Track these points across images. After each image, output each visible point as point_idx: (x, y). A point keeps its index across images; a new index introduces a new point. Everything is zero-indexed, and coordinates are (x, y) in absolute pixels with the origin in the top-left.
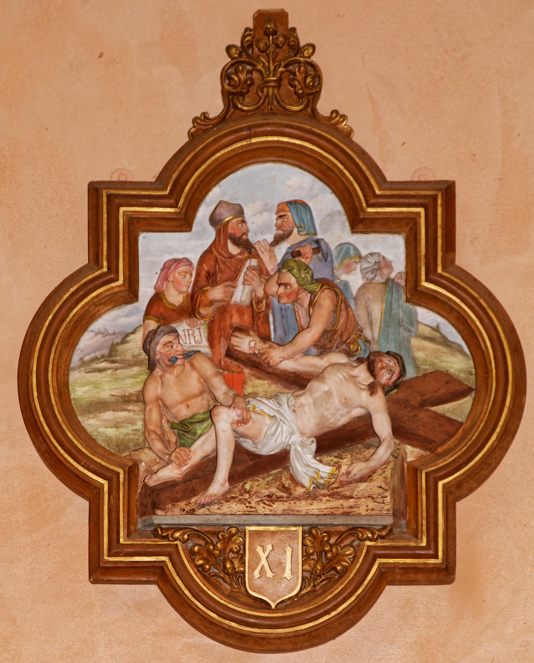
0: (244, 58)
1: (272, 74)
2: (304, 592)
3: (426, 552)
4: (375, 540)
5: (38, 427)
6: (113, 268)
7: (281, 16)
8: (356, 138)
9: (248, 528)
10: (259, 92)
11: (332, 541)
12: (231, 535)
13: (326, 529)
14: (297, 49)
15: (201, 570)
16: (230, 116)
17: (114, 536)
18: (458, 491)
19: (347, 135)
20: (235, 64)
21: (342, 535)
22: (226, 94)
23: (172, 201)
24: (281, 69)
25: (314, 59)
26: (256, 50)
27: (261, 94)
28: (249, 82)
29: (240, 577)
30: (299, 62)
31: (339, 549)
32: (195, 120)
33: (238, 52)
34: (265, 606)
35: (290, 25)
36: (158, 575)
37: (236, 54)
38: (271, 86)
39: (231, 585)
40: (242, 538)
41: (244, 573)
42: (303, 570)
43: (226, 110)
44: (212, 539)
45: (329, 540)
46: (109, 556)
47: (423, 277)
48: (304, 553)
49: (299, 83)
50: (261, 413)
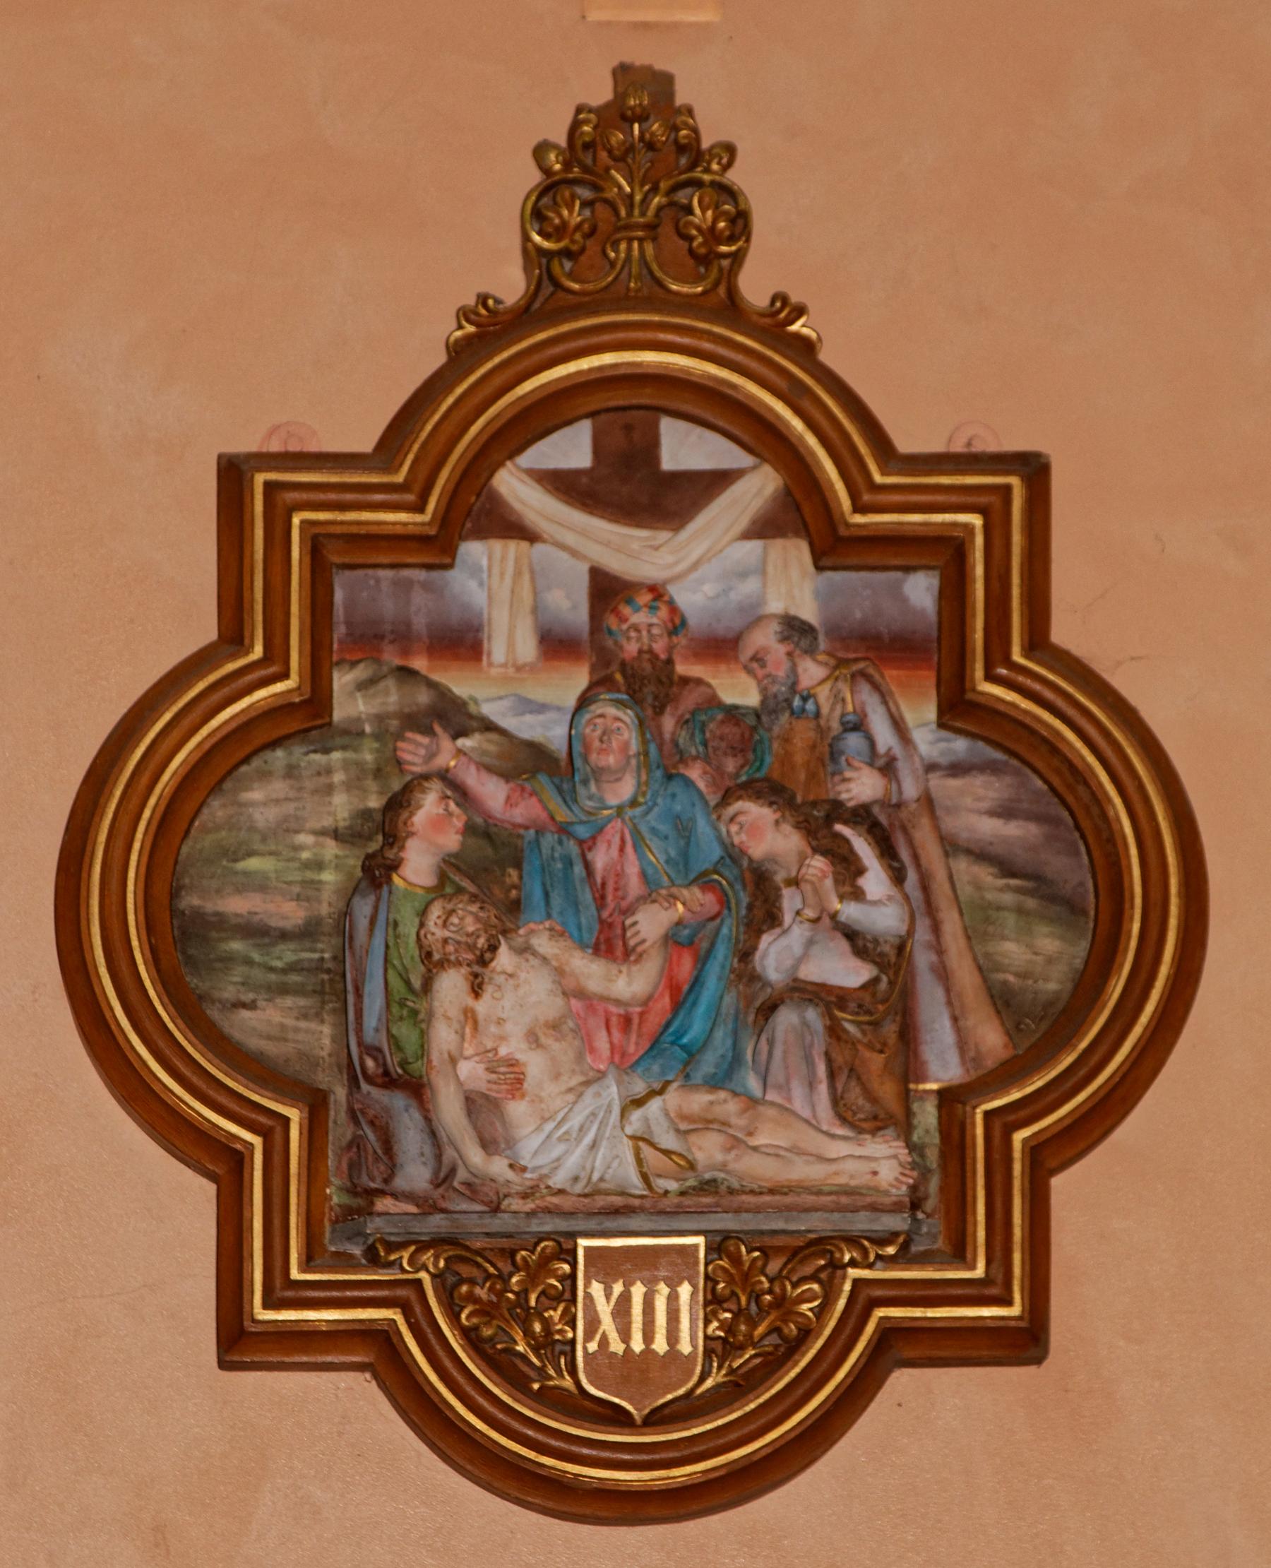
1: (636, 212)
2: (699, 1391)
4: (870, 1266)
7: (663, 83)
9: (583, 1243)
14: (692, 152)
16: (543, 304)
17: (278, 1263)
19: (805, 349)
20: (551, 188)
22: (532, 256)
23: (410, 497)
25: (734, 177)
27: (613, 255)
29: (562, 1353)
30: (698, 184)
34: (618, 1418)
35: (680, 100)
38: (635, 199)
40: (568, 1263)
41: (573, 1342)
42: (706, 1337)
44: (500, 1265)
45: (765, 1265)
46: (266, 1305)
47: (979, 672)
48: (709, 1297)
49: (699, 229)
50: (252, 804)
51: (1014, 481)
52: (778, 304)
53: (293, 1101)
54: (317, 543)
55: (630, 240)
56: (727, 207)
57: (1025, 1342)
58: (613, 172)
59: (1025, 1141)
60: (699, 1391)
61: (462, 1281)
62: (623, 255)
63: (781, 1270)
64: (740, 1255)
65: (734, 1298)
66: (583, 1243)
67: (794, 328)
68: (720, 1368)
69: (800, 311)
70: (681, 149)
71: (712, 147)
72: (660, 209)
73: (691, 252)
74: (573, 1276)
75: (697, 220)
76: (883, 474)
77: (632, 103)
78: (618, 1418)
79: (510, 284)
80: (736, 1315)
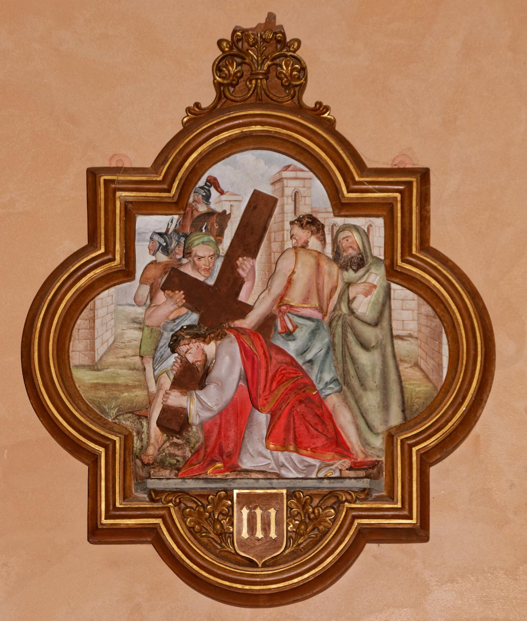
0: (235, 50)
2: (284, 554)
3: (401, 513)
5: (68, 310)
6: (110, 249)
8: (339, 128)
10: (248, 83)
11: (316, 502)
12: (221, 499)
13: (309, 493)
15: (191, 529)
16: (222, 106)
18: (427, 460)
19: (330, 125)
21: (324, 497)
22: (218, 86)
24: (269, 63)
25: (299, 53)
26: (246, 45)
28: (239, 74)
30: (286, 56)
31: (321, 510)
32: (188, 110)
33: (228, 46)
34: (252, 564)
36: (151, 536)
37: (227, 47)
39: (220, 545)
43: (219, 98)
48: (289, 515)
51: (413, 179)
52: (318, 106)
53: (116, 433)
54: (391, 497)
55: (257, 79)
56: (297, 66)
57: (420, 533)
58: (250, 51)
59: (418, 451)
60: (284, 554)
61: (187, 507)
62: (254, 86)
63: (318, 504)
64: (300, 497)
65: (401, 328)
66: (236, 492)
67: (326, 115)
68: (294, 543)
69: (327, 109)
70: (278, 42)
71: (291, 41)
72: (269, 67)
73: (282, 85)
74: (232, 506)
75: (284, 72)
76: (361, 176)
77: (506, 23)
78: (252, 564)
79: (207, 98)
80: (301, 522)
